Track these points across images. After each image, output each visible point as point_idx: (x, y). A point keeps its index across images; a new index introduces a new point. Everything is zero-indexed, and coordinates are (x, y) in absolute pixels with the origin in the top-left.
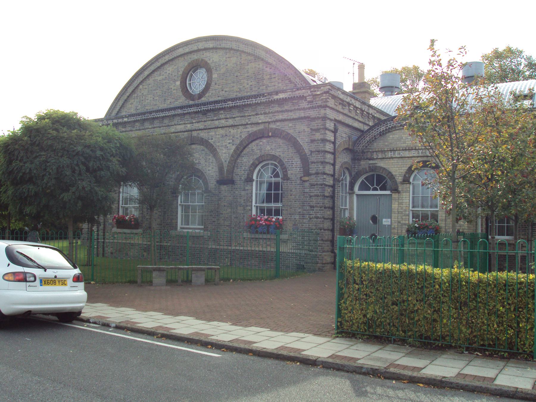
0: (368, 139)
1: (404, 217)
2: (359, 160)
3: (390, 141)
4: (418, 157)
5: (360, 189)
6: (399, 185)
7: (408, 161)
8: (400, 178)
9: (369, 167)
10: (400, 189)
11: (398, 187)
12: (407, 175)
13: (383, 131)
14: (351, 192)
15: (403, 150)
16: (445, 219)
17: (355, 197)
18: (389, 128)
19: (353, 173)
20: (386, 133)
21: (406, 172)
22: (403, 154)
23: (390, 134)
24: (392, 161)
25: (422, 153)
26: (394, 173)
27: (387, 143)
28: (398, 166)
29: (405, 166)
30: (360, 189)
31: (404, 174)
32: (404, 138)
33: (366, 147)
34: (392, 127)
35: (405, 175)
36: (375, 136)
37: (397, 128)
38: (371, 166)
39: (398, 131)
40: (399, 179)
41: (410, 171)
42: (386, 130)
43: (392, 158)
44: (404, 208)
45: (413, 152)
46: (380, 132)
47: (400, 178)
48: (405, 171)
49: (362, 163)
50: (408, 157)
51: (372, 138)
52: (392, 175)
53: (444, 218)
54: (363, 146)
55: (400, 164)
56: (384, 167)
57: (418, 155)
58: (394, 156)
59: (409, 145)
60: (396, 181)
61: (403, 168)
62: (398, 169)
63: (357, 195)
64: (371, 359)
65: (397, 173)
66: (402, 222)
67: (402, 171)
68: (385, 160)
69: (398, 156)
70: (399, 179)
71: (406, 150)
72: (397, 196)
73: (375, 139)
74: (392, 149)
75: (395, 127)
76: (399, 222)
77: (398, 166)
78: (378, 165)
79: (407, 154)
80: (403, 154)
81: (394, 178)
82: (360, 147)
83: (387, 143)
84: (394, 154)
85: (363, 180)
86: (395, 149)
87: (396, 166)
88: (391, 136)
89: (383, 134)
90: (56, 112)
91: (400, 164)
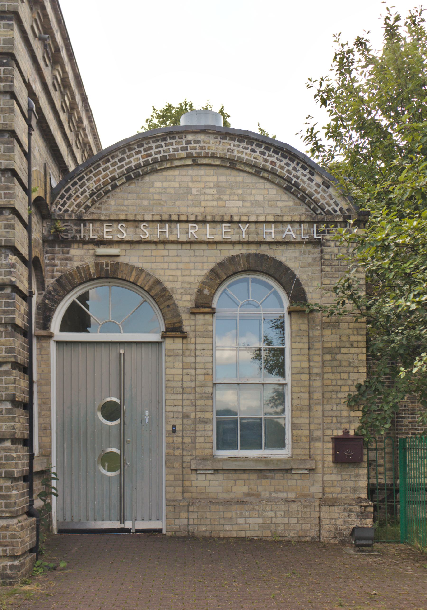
0: (92, 185)
1: (199, 402)
2: (67, 243)
3: (156, 197)
4: (233, 243)
5: (65, 327)
6: (184, 316)
7: (208, 252)
8: (187, 298)
9: (97, 265)
10: (186, 329)
11: (181, 322)
12: (206, 292)
13: (138, 166)
14: (43, 333)
15: (196, 222)
16: (309, 405)
17: (53, 346)
18: (155, 161)
19: (49, 282)
20: (146, 174)
21: (203, 283)
22: (194, 232)
23: (154, 177)
24: (161, 251)
25: (248, 233)
26: (168, 285)
27: (146, 203)
28: (180, 266)
29: (199, 266)
30: (65, 327)
31: (195, 287)
32: (194, 191)
33: (87, 208)
34: (164, 159)
35: (200, 291)
36: (113, 179)
37: (176, 163)
38: (103, 261)
39: (176, 172)
40: (184, 301)
41: (221, 274)
42: (147, 164)
43: (164, 242)
44: (200, 378)
45: (224, 228)
46: (129, 170)
47: (187, 298)
48: (200, 279)
49: (75, 252)
50: (208, 243)
51: (105, 184)
52: (164, 289)
53: (306, 402)
54: (78, 206)
55: (186, 259)
56: (140, 265)
57: (236, 238)
58: (172, 238)
59: (208, 210)
60: (176, 306)
61: (193, 272)
62: (179, 273)
63: (58, 343)
64: (333, 115)
65: (178, 285)
66: (193, 415)
67: (192, 279)
68: (142, 246)
69: (183, 238)
70: (184, 301)
71: (204, 222)
72: (180, 346)
73: (115, 187)
74: (165, 217)
75: (172, 159)
76: (186, 416)
77: (180, 266)
78: (121, 260)
79: (208, 233)
80: (194, 232)
81: (170, 297)
82: (71, 206)
83: (146, 203)
84: (171, 232)
85: (74, 303)
86: (175, 218)
87: (174, 266)
88: (158, 184)
89: (138, 176)
90: (287, 145)
91: (186, 259)
